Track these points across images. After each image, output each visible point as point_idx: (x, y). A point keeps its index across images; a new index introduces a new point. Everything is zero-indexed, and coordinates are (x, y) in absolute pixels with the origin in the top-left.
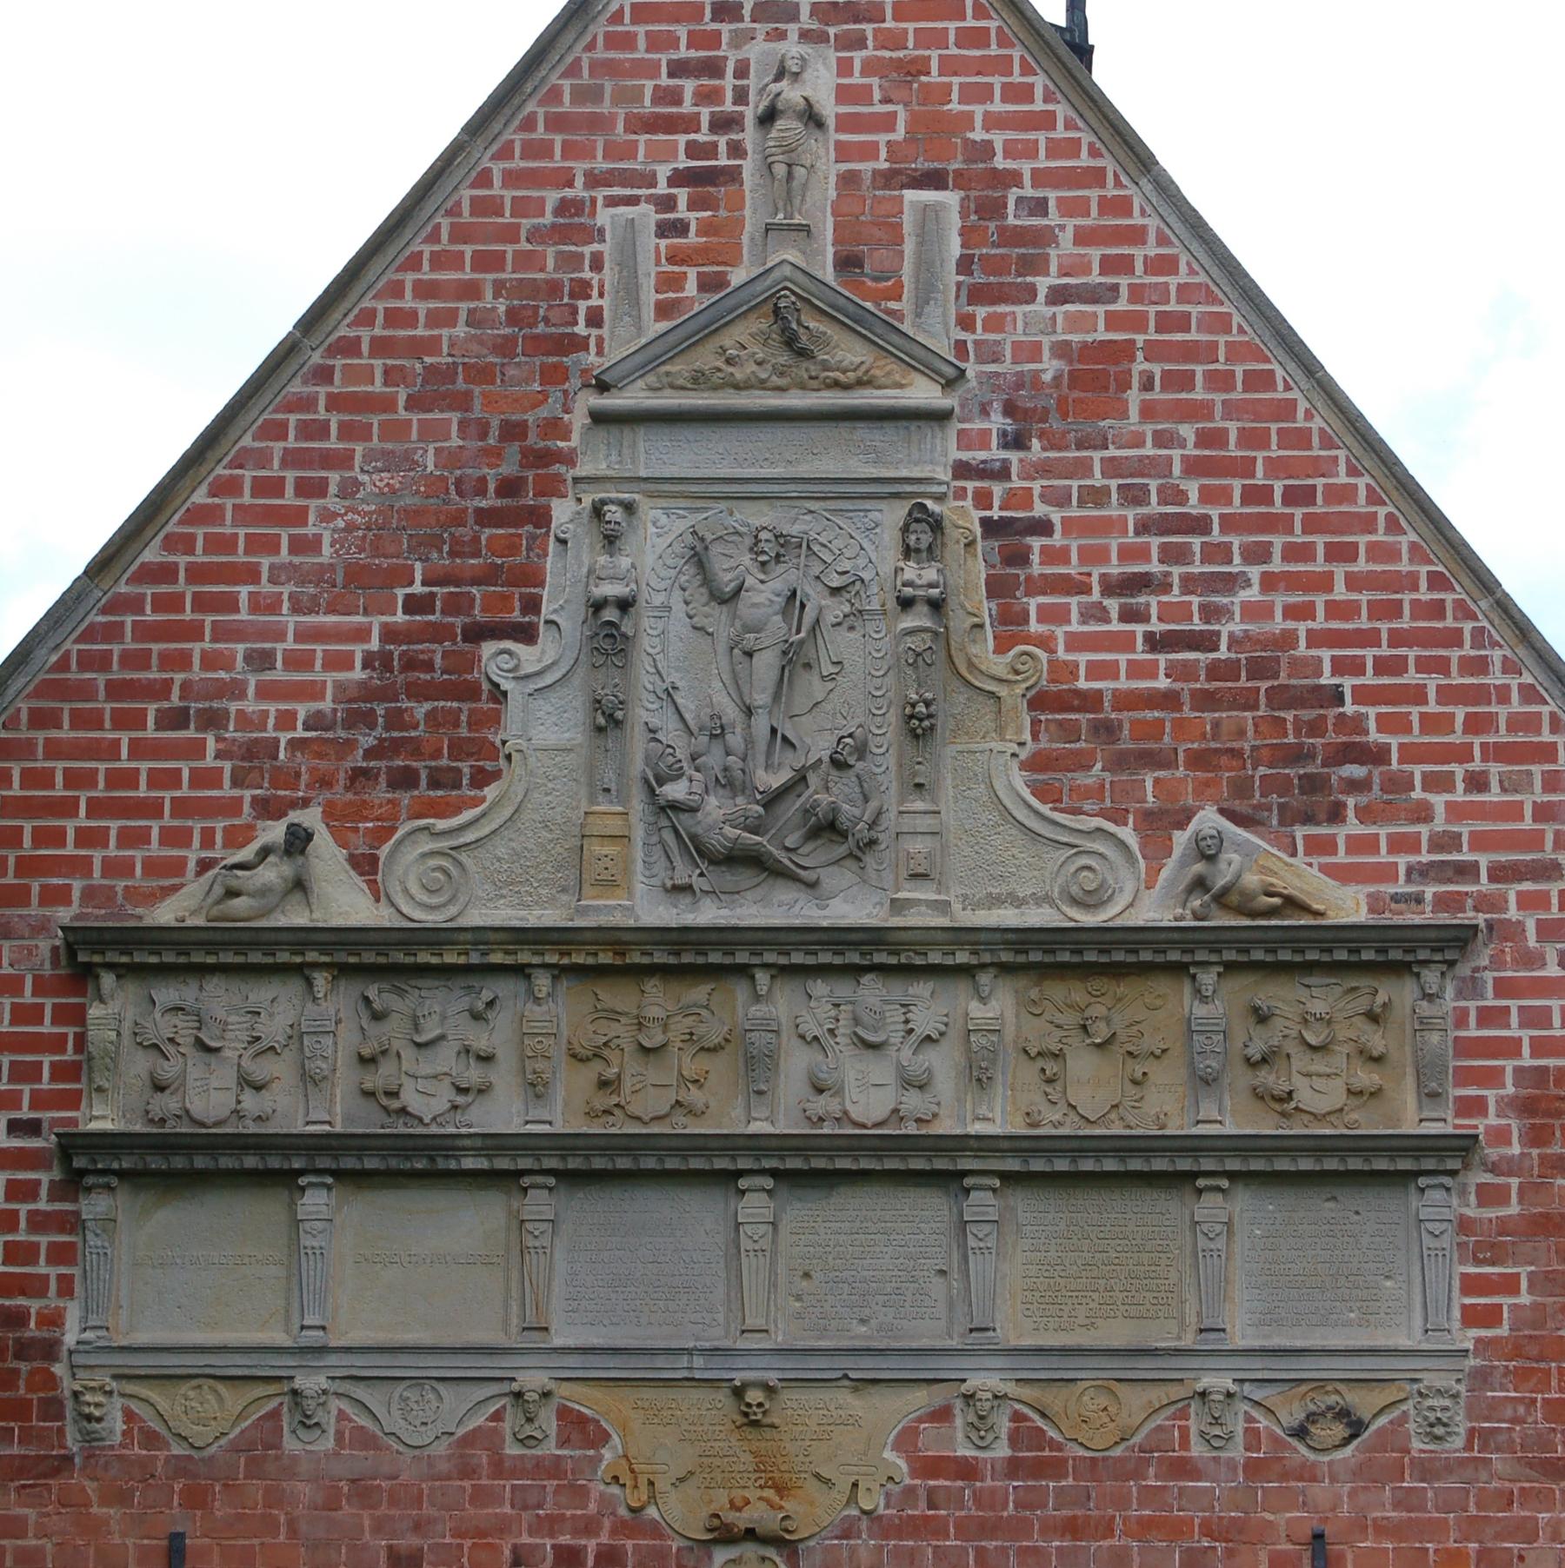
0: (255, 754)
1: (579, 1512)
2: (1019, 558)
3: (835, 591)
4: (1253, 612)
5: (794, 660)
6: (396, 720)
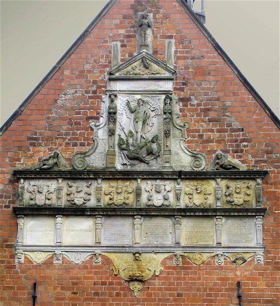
3: (152, 111)
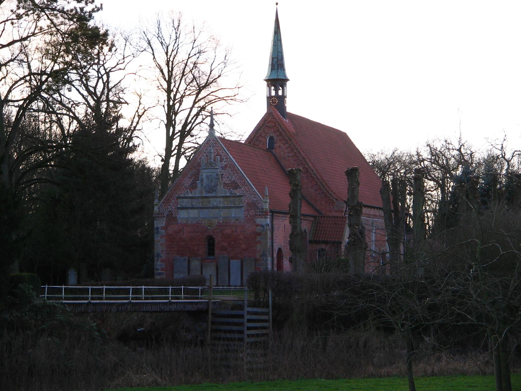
0: (186, 187)
1: (488, 264)
2: (222, 176)
4: (234, 179)
5: (211, 181)
6: (192, 185)
